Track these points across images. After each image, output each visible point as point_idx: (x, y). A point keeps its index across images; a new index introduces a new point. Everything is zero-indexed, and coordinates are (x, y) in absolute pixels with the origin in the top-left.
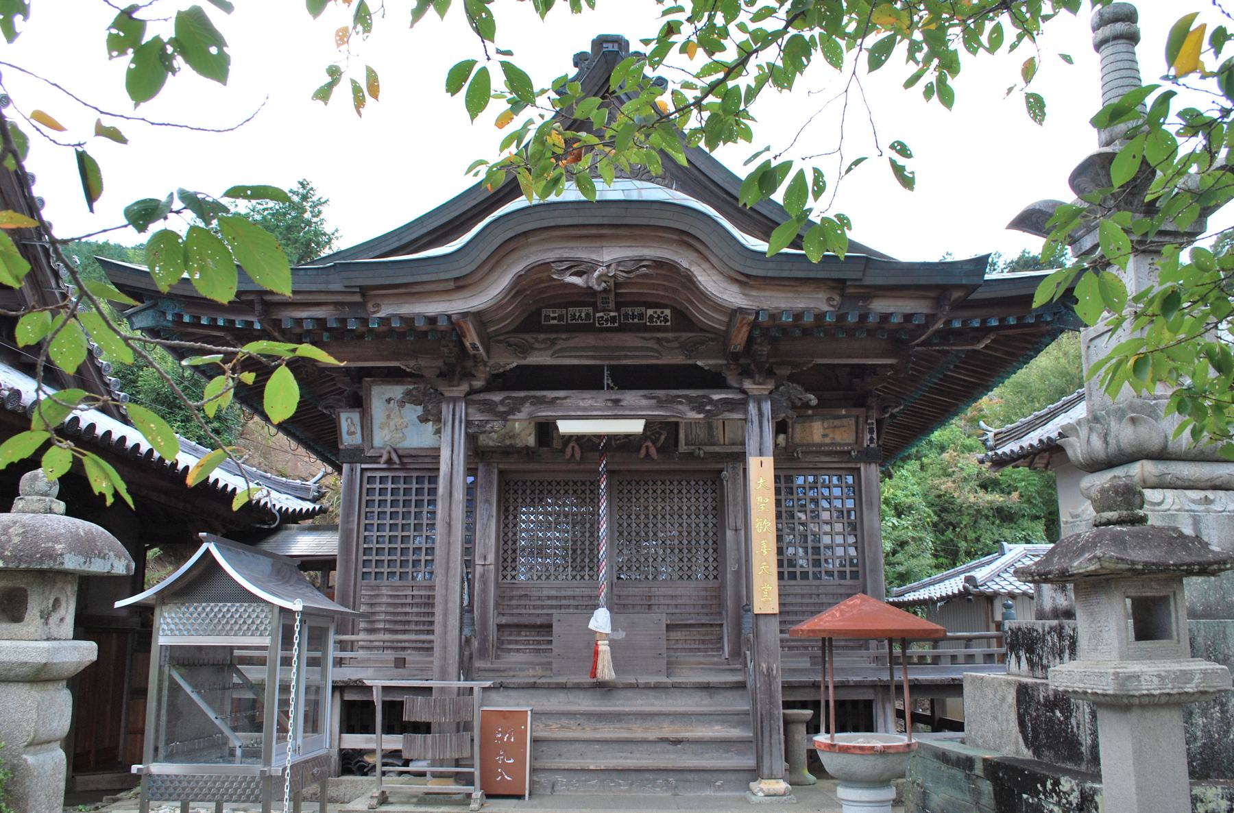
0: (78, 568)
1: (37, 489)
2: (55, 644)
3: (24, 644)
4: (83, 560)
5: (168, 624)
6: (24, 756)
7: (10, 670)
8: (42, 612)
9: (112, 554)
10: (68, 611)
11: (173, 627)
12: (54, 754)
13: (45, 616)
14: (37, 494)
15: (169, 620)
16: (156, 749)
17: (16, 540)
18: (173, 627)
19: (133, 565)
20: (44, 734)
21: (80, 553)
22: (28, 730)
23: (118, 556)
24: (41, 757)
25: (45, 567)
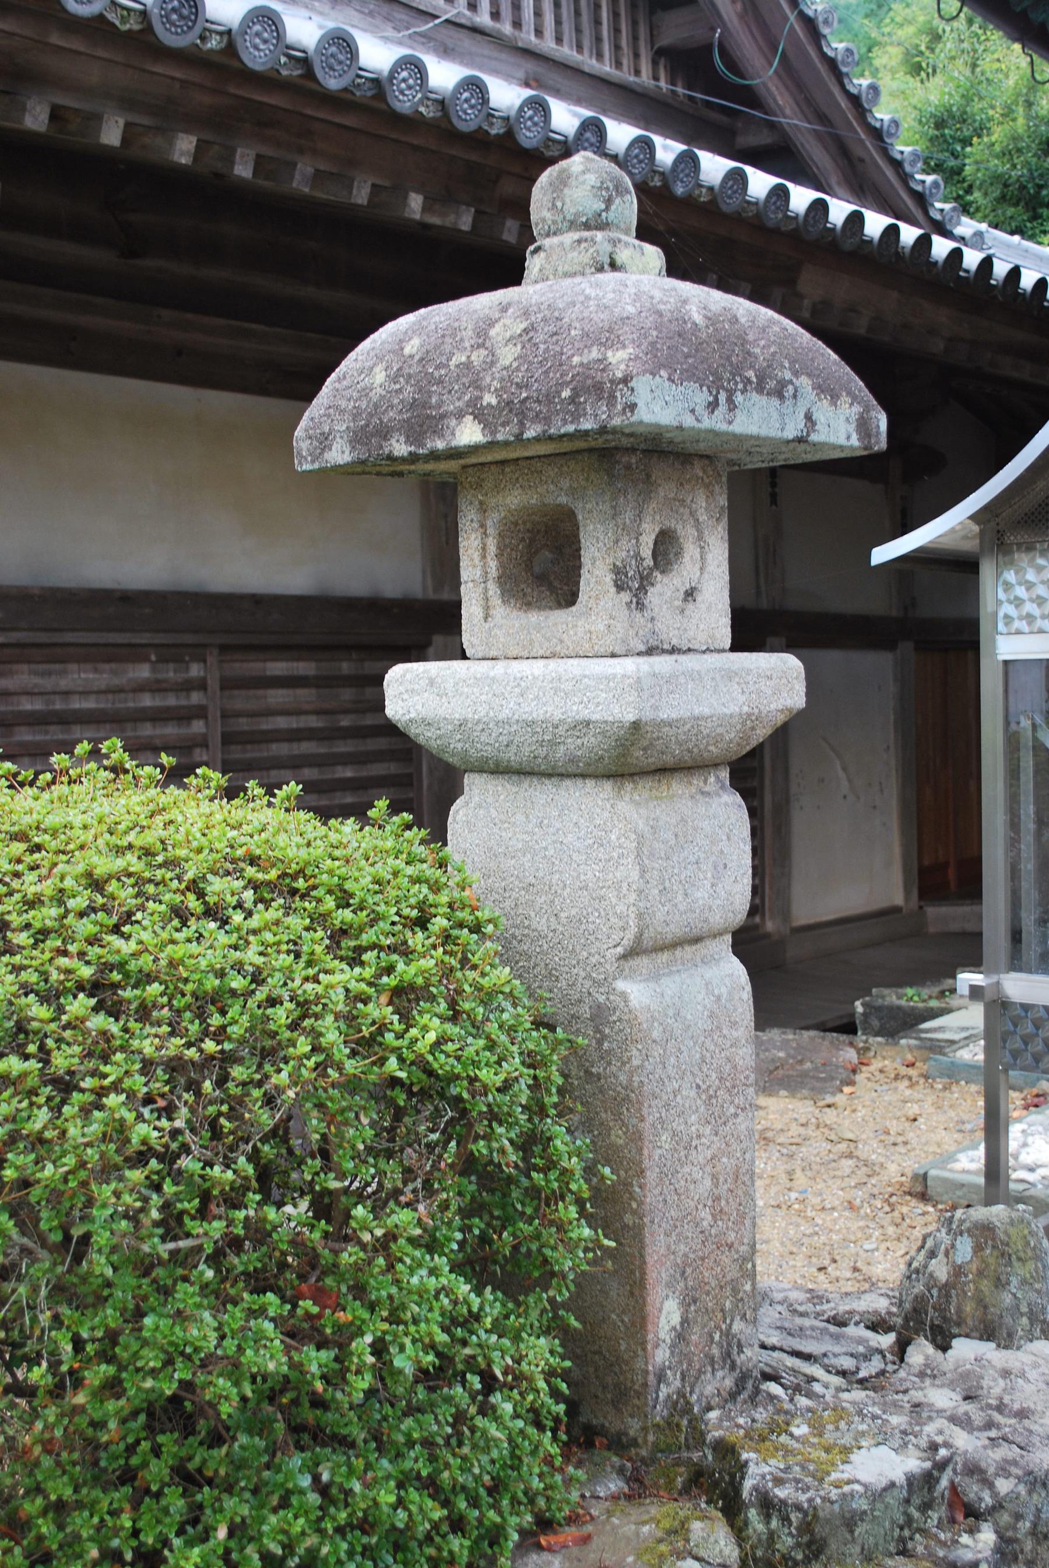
0: (689, 421)
1: (570, 211)
2: (662, 663)
3: (574, 666)
4: (702, 397)
5: (1018, 602)
6: (621, 985)
7: (553, 744)
8: (618, 571)
9: (804, 382)
10: (708, 568)
11: (1030, 608)
12: (710, 973)
13: (634, 584)
14: (573, 225)
15: (1021, 592)
16: (1016, 936)
17: (508, 356)
18: (1030, 608)
19: (882, 421)
20: (669, 921)
21: (690, 375)
22: (615, 922)
23: (828, 391)
24: (670, 986)
25: (587, 425)
